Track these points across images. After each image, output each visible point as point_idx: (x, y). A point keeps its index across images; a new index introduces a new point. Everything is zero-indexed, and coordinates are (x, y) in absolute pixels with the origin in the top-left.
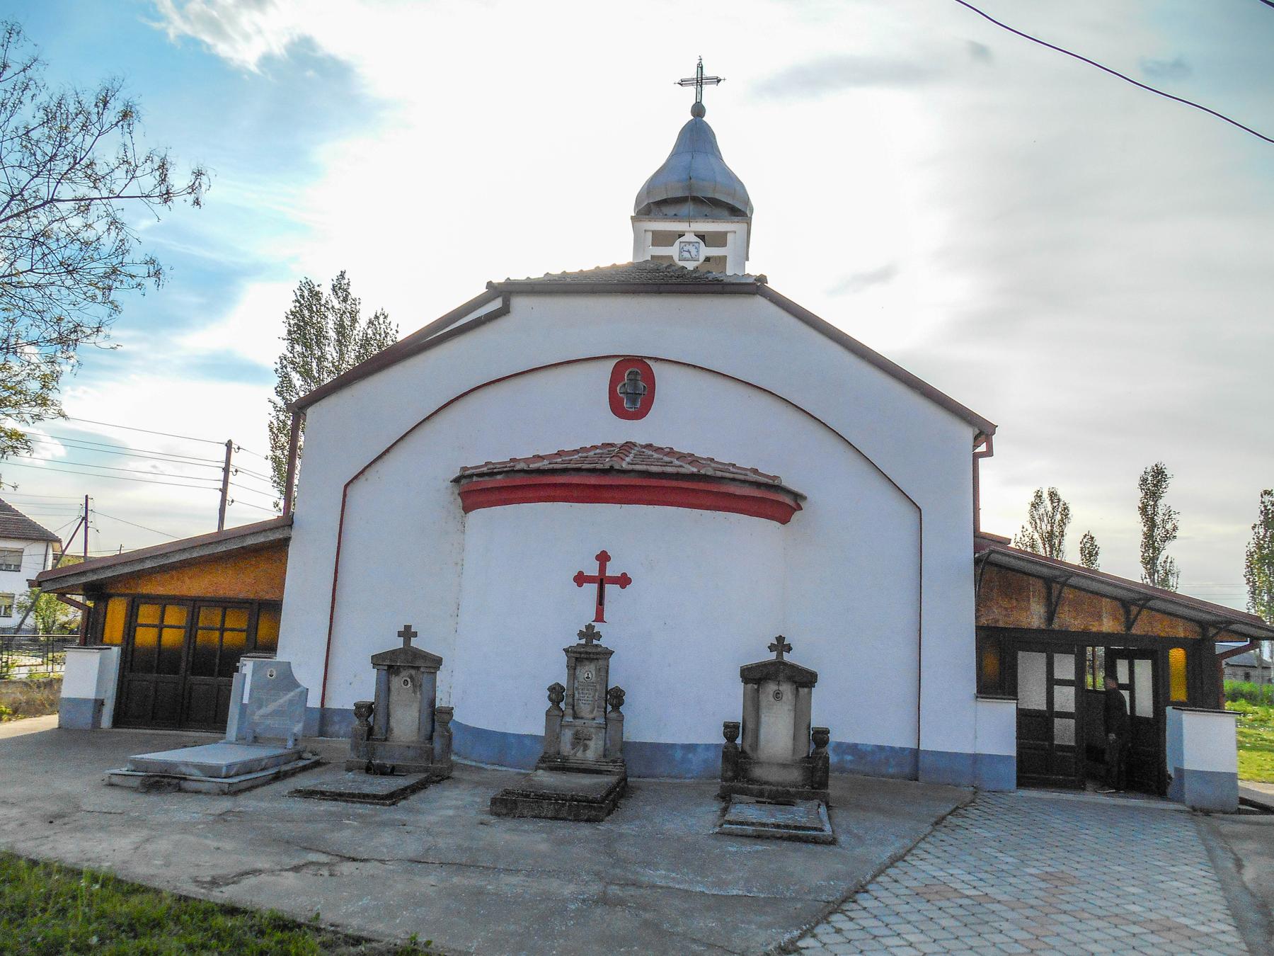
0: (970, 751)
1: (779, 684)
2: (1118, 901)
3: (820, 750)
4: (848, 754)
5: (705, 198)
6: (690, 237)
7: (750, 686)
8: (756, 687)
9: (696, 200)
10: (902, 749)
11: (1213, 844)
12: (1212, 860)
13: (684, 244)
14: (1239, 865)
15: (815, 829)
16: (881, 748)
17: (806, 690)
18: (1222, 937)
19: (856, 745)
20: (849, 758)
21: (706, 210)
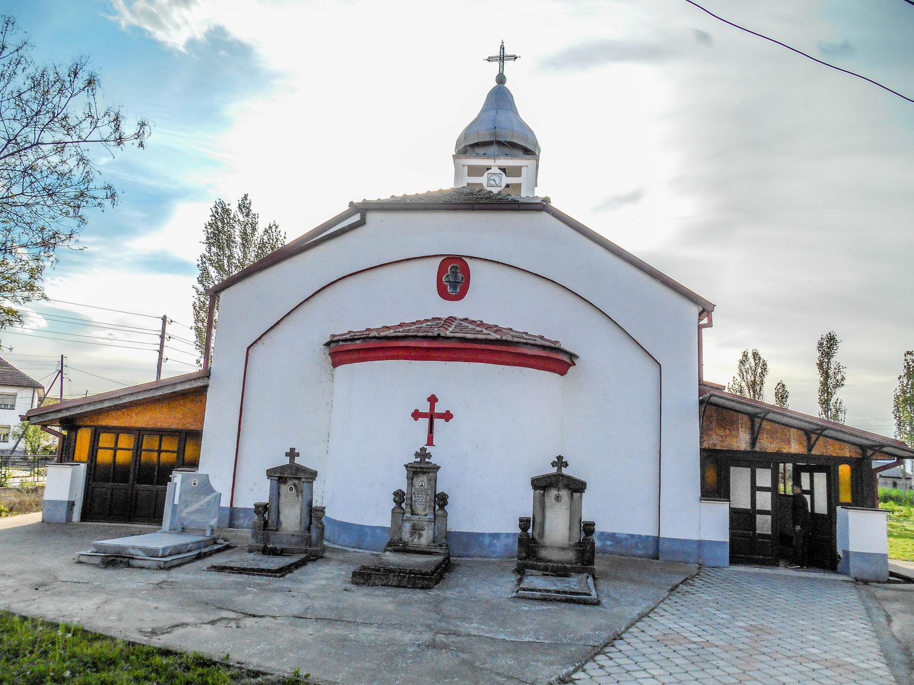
0: (696, 538)
1: (559, 491)
2: (802, 645)
3: (588, 538)
4: (609, 540)
5: (506, 142)
6: (495, 170)
7: (538, 491)
8: (542, 492)
9: (500, 143)
10: (647, 537)
11: (870, 605)
12: (869, 616)
13: (491, 175)
14: (889, 619)
15: (585, 594)
16: (632, 536)
17: (578, 494)
18: (876, 671)
19: (614, 534)
20: (609, 543)
21: (507, 150)
